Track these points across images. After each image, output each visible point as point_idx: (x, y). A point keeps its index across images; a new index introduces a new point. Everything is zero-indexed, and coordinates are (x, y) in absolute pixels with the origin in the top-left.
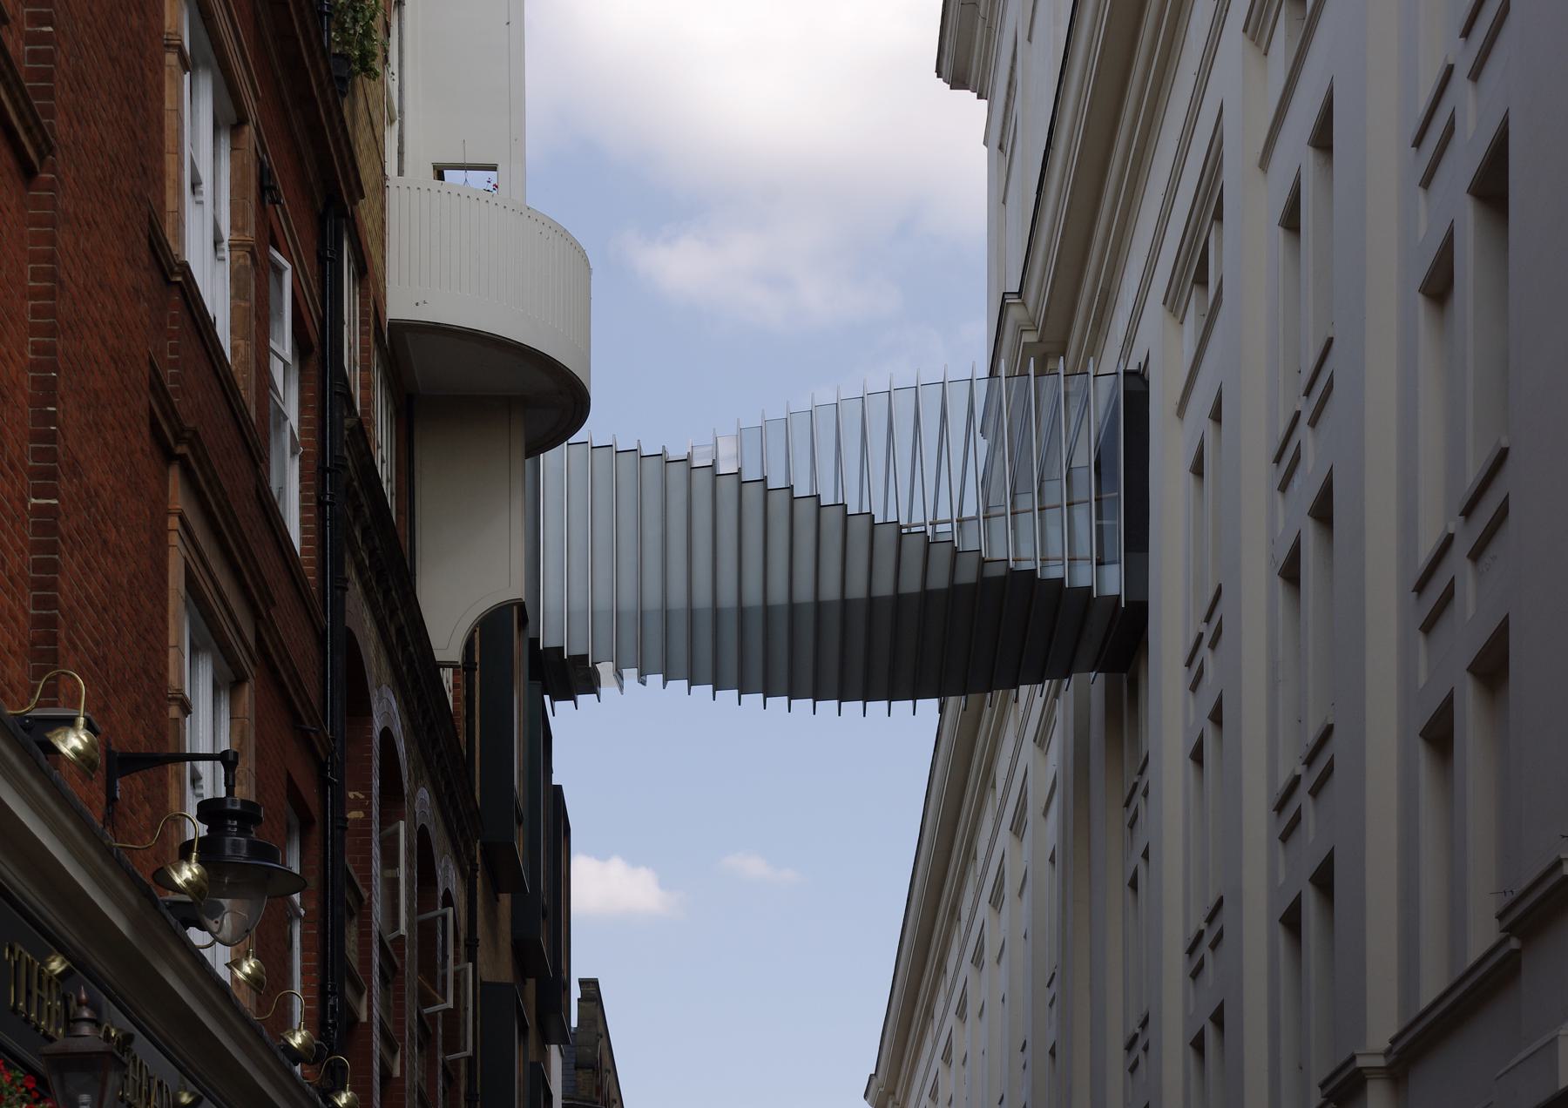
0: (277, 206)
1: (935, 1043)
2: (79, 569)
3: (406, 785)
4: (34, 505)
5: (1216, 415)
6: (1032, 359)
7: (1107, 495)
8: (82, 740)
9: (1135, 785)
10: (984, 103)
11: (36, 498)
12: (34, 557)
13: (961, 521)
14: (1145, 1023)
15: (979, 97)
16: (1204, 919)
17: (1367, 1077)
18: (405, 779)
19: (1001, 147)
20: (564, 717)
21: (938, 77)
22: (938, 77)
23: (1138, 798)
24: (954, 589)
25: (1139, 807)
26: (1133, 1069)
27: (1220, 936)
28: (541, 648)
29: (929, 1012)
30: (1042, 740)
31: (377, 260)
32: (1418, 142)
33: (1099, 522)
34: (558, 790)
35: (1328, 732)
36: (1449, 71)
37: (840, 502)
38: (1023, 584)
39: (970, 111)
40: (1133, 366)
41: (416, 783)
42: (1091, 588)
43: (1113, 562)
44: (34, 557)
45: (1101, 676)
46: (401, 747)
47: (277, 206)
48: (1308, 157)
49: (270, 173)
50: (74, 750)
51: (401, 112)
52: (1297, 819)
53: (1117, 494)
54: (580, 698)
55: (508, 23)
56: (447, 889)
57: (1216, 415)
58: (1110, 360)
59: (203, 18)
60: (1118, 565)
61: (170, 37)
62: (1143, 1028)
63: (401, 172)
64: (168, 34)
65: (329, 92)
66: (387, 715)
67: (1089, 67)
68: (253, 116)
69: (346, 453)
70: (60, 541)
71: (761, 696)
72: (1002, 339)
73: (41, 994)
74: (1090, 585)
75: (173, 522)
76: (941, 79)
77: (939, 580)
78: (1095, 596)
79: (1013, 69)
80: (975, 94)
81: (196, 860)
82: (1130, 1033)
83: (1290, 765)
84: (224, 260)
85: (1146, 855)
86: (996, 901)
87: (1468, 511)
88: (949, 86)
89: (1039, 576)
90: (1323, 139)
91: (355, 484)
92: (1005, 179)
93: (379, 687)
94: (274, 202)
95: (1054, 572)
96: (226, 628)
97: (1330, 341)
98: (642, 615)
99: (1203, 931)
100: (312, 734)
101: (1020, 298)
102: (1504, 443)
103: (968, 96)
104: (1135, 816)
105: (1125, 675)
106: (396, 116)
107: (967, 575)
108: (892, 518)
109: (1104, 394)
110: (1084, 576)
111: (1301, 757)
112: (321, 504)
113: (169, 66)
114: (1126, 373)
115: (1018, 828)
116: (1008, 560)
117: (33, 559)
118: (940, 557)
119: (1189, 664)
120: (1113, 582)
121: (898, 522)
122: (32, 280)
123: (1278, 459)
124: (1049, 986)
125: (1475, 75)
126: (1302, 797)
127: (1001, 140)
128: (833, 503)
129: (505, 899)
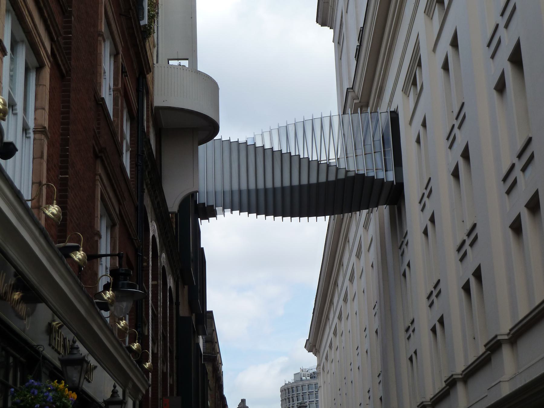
0: (126, 77)
1: (330, 328)
2: (74, 197)
3: (159, 253)
4: (60, 177)
5: (424, 125)
6: (359, 108)
7: (387, 149)
8: (81, 256)
9: (403, 242)
10: (332, 30)
11: (61, 175)
12: (60, 194)
13: (338, 159)
14: (413, 322)
15: (331, 28)
16: (433, 287)
17: (502, 342)
18: (159, 251)
19: (338, 43)
20: (205, 226)
21: (317, 23)
22: (317, 23)
23: (404, 246)
24: (337, 181)
25: (405, 249)
26: (409, 338)
27: (440, 292)
28: (198, 203)
29: (327, 318)
30: (366, 226)
31: (151, 89)
32: (489, 45)
33: (385, 158)
34: (203, 248)
35: (474, 226)
36: (497, 26)
37: (289, 152)
38: (360, 178)
39: (328, 33)
40: (392, 109)
41: (162, 252)
42: (383, 179)
43: (390, 170)
44: (60, 194)
45: (388, 207)
46: (158, 240)
47: (126, 77)
48: (450, 50)
49: (125, 67)
50: (79, 259)
51: (158, 44)
52: (465, 254)
53: (390, 149)
54: (210, 219)
55: (192, 18)
56: (170, 286)
57: (424, 125)
58: (384, 107)
59: (108, 25)
60: (392, 171)
61: (100, 32)
62: (412, 325)
63: (157, 62)
64: (99, 31)
65: (142, 43)
66: (154, 231)
67: (373, 23)
68: (121, 52)
69: (144, 149)
70: (68, 188)
71: (273, 216)
72: (347, 102)
73: (58, 339)
74: (393, 180)
75: (98, 177)
76: (318, 24)
77: (332, 178)
78: (385, 181)
79: (341, 21)
80: (329, 28)
81: (111, 290)
82: (407, 326)
83: (462, 236)
84: (111, 94)
85: (409, 265)
86: (351, 280)
87: (520, 156)
88: (321, 26)
89: (366, 176)
90: (454, 43)
91: (147, 158)
92: (340, 53)
93: (151, 222)
94: (125, 76)
95: (371, 174)
96: (111, 209)
97: (463, 104)
98: (232, 192)
99: (432, 291)
100: (134, 240)
101: (352, 89)
102: (530, 136)
103: (327, 29)
104: (403, 252)
105: (396, 206)
106: (156, 45)
107: (342, 176)
108: (306, 156)
109: (384, 118)
110: (381, 175)
111: (465, 234)
112: (137, 165)
113: (99, 40)
114: (390, 111)
115: (358, 256)
116: (355, 171)
117: (60, 194)
118: (332, 171)
119: (420, 202)
120: (391, 177)
121: (317, 160)
122: (62, 108)
123: (448, 139)
124: (374, 309)
125: (506, 26)
126: (467, 246)
127: (339, 41)
128: (286, 152)
129: (186, 287)
